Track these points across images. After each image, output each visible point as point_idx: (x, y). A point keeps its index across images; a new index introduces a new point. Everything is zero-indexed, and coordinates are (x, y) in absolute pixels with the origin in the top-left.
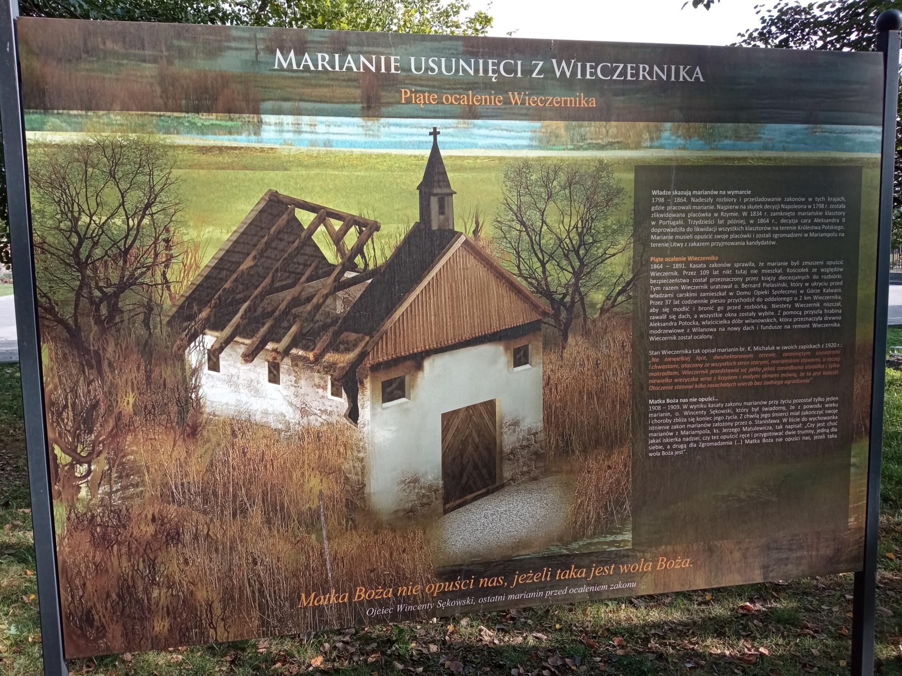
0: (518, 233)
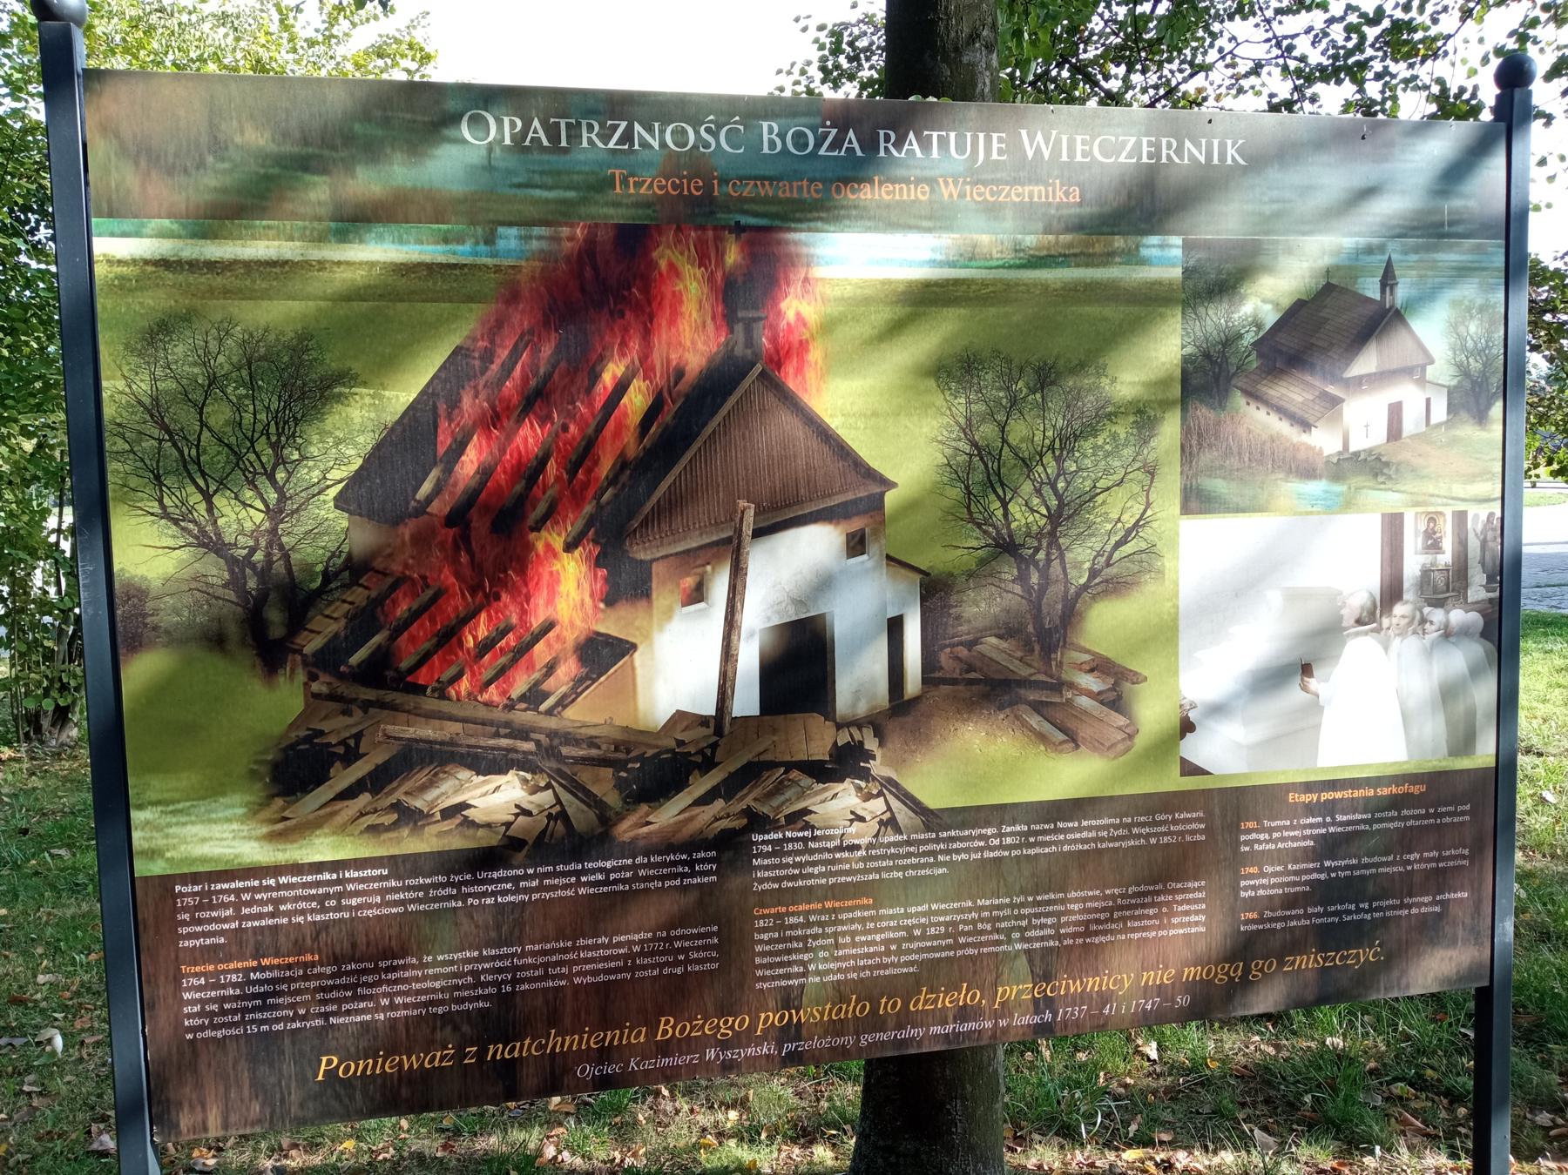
0: (155, 443)
